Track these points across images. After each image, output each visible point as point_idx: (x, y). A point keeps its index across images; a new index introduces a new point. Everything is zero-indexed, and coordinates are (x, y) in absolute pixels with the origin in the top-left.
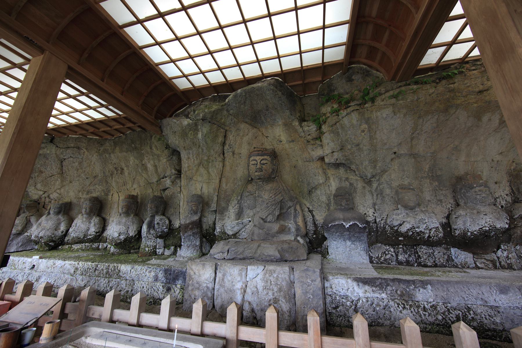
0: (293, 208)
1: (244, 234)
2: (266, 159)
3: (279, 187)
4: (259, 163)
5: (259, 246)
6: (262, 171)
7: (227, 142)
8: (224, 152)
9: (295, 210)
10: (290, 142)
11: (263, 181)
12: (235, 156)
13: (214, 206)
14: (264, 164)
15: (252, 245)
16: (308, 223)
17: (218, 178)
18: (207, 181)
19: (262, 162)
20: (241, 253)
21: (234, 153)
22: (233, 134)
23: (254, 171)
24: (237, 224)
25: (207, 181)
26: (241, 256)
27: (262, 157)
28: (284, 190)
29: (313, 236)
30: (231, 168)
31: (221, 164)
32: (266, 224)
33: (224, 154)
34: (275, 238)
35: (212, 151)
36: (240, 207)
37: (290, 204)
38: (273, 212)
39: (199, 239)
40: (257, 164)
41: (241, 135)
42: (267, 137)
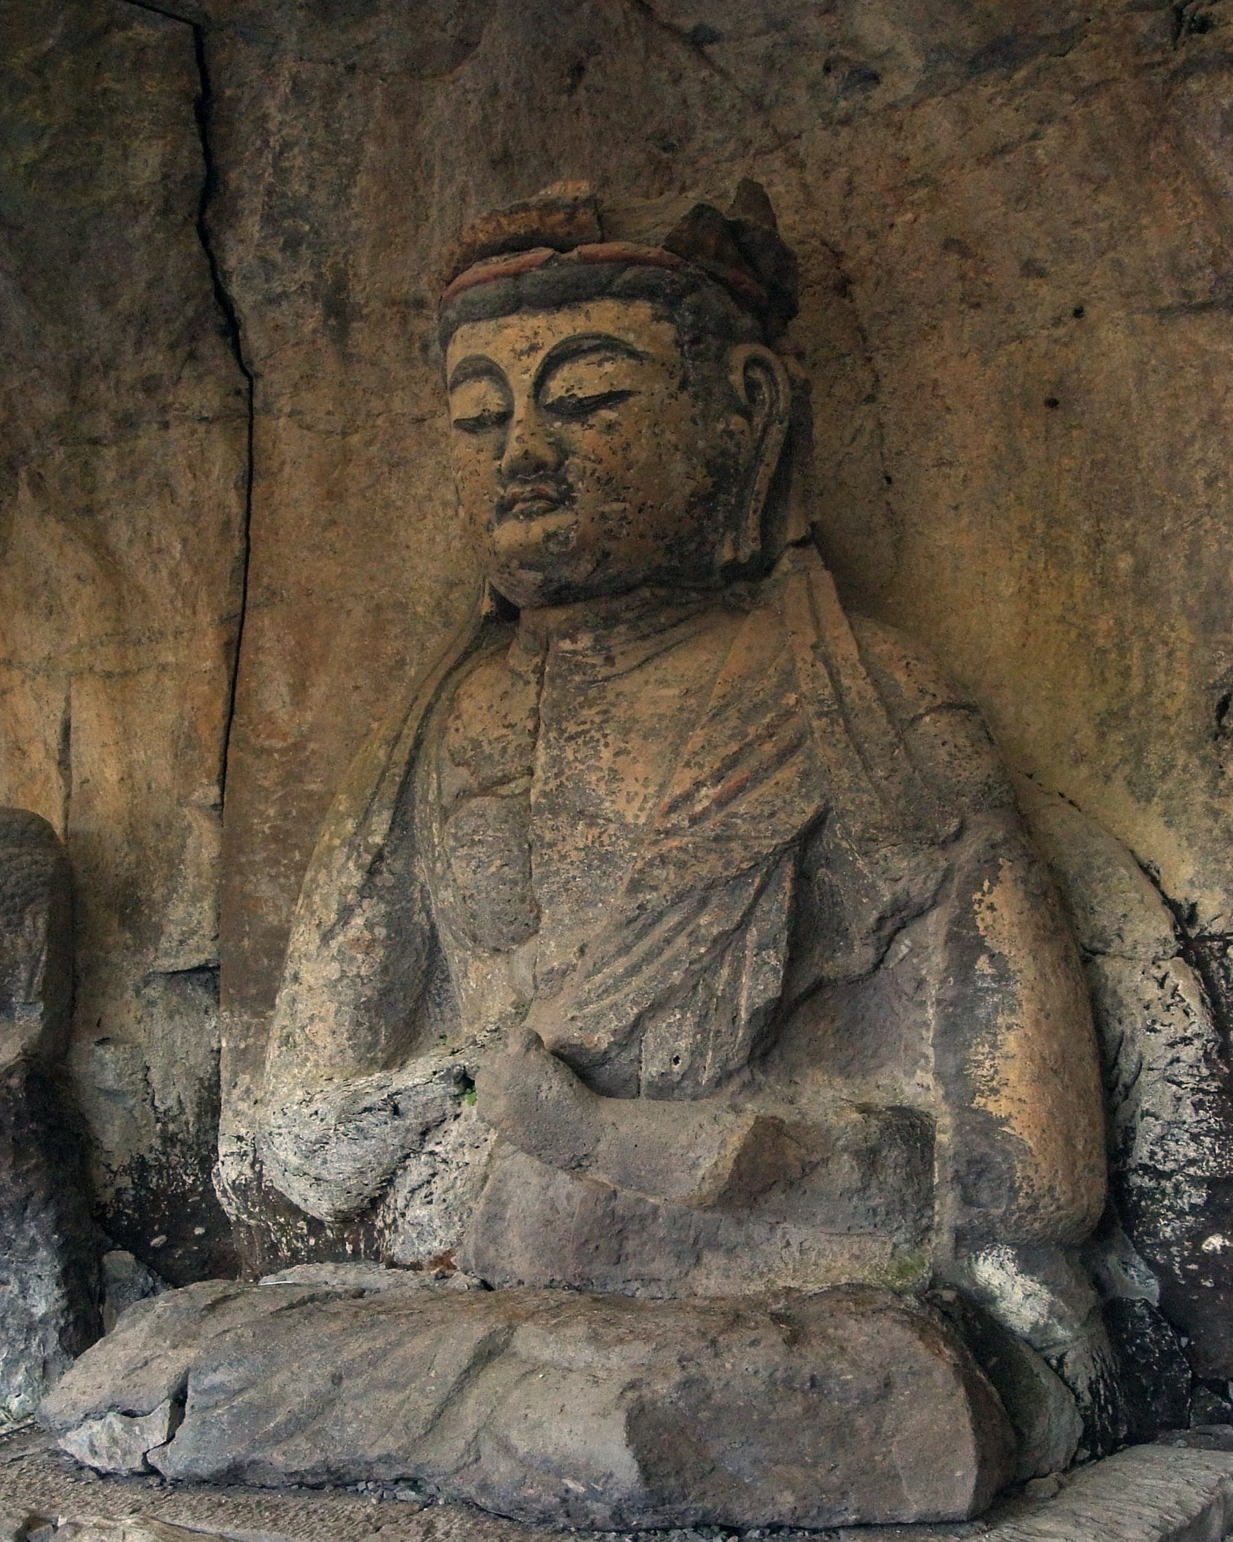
0: (936, 924)
1: (421, 1223)
2: (608, 346)
3: (788, 680)
4: (521, 407)
5: (487, 1354)
6: (564, 500)
7: (248, 181)
8: (225, 304)
9: (965, 944)
10: (976, 65)
11: (610, 621)
12: (361, 338)
13: (187, 926)
14: (580, 409)
15: (418, 1345)
16: (1154, 1096)
17: (205, 618)
18: (107, 658)
19: (556, 387)
20: (297, 1425)
21: (339, 310)
22: (288, 67)
24: (345, 1117)
25: (107, 658)
26: (301, 1456)
28: (839, 708)
29: (1198, 1237)
30: (335, 494)
31: (222, 458)
32: (608, 1110)
33: (232, 329)
34: (713, 1260)
35: (89, 308)
36: (398, 924)
37: (899, 872)
38: (702, 972)
39: (46, 1264)
40: (503, 418)
41: (390, 60)
42: (699, 40)
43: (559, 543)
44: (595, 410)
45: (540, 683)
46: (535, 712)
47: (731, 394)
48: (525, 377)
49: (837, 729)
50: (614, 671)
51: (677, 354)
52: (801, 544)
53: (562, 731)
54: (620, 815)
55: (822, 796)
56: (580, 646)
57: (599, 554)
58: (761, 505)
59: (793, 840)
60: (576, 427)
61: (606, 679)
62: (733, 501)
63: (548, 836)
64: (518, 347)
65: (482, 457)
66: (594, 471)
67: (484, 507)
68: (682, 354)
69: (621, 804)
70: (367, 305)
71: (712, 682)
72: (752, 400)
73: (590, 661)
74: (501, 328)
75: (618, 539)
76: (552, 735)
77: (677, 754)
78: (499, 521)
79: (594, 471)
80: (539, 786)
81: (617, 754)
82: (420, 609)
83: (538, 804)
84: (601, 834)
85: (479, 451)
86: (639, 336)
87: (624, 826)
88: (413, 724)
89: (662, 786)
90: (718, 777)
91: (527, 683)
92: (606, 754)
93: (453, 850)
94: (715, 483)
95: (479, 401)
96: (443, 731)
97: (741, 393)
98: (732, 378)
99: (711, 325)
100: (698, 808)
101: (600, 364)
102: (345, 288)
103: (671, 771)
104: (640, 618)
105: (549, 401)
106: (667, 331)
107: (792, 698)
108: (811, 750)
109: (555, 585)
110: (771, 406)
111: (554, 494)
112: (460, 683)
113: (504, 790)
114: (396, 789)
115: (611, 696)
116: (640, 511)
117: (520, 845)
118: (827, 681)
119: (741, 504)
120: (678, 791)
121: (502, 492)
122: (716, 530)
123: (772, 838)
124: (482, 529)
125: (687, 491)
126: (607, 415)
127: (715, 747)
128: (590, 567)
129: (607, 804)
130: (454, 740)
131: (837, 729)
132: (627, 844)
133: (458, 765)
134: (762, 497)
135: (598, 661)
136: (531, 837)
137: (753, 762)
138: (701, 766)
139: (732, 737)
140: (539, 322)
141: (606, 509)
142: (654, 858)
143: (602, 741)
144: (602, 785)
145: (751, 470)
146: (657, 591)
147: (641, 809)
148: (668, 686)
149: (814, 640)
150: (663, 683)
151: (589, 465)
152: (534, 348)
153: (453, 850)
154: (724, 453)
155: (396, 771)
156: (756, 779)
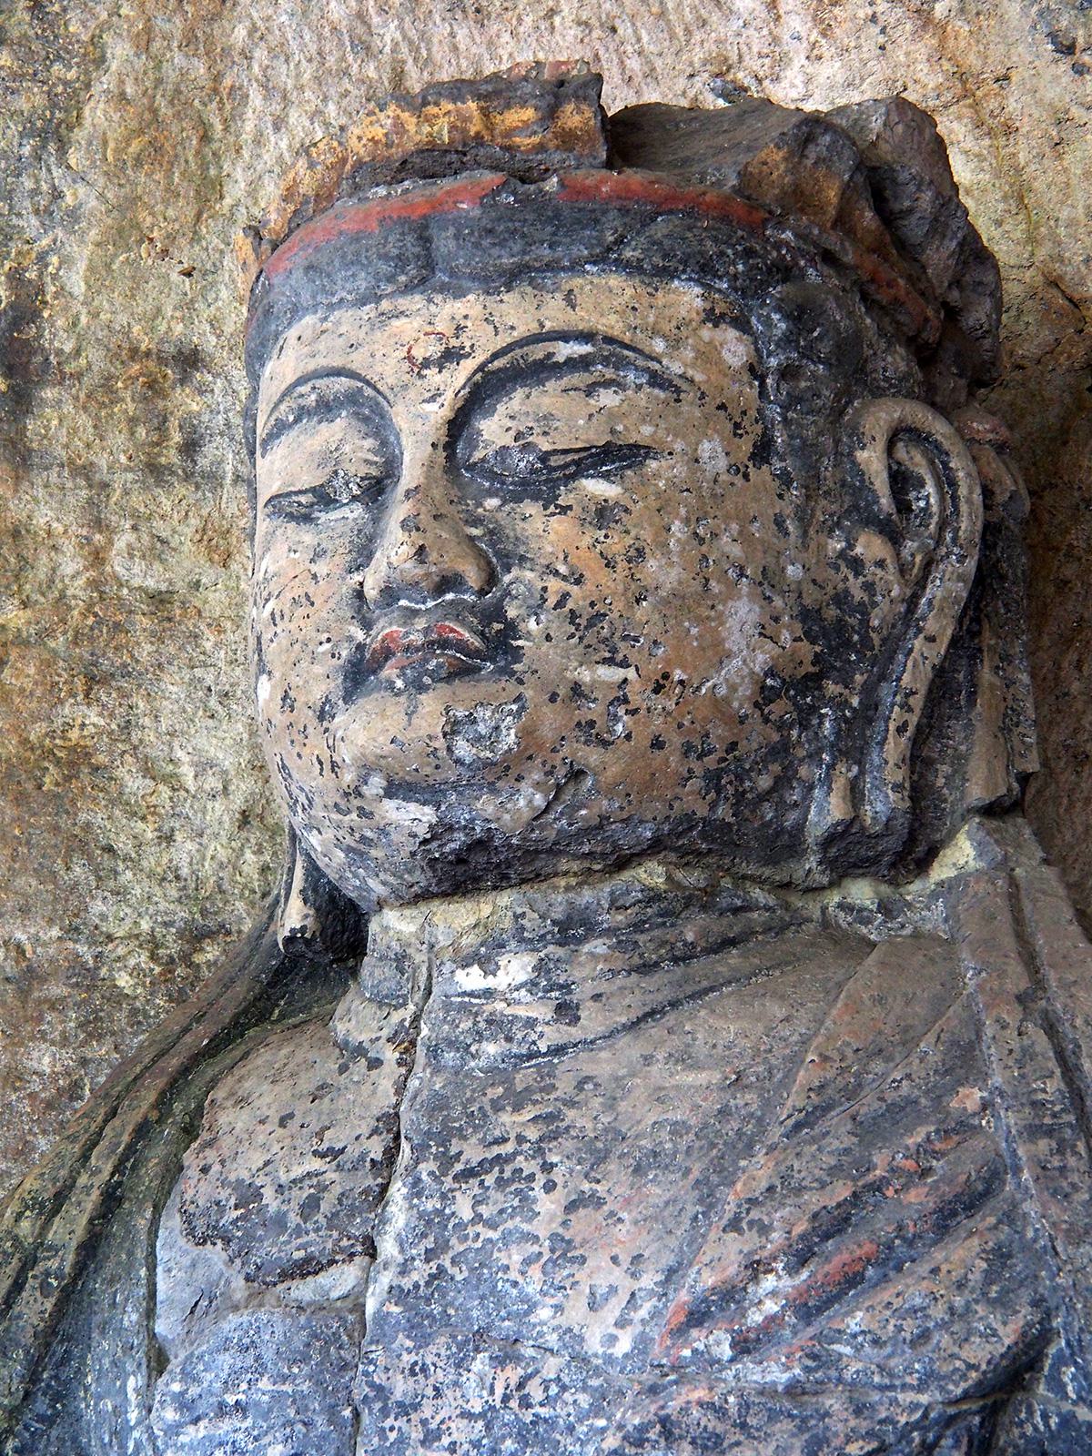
11: (572, 930)
14: (547, 479)
23: (320, 682)
27: (518, 313)
40: (376, 490)
43: (478, 740)
44: (573, 477)
45: (406, 1063)
46: (390, 1122)
47: (858, 488)
48: (433, 407)
49: (1072, 1161)
50: (575, 1033)
51: (752, 392)
52: (991, 811)
53: (447, 1161)
54: (572, 1337)
55: (1035, 1304)
56: (500, 981)
57: (561, 772)
58: (914, 719)
59: (966, 1396)
60: (531, 508)
61: (559, 1050)
62: (855, 702)
63: (401, 1387)
64: (419, 353)
65: (321, 568)
66: (565, 596)
67: (318, 669)
68: (763, 393)
69: (576, 1313)
70: (77, 352)
71: (795, 1060)
72: (903, 507)
73: (522, 1012)
74: (385, 317)
75: (605, 744)
76: (425, 1169)
77: (709, 1202)
78: (348, 697)
79: (565, 596)
80: (386, 1279)
81: (571, 1207)
82: (124, 981)
83: (381, 1318)
84: (528, 1377)
85: (318, 554)
86: (675, 343)
87: (580, 1359)
88: (103, 1164)
89: (672, 1274)
90: (801, 1256)
91: (375, 1064)
92: (548, 1205)
93: (174, 1430)
94: (817, 659)
95: (330, 458)
96: (174, 1170)
97: (881, 484)
98: (862, 456)
99: (825, 348)
100: (755, 1318)
101: (590, 391)
102: (35, 315)
103: (695, 1241)
104: (638, 927)
105: (478, 455)
106: (734, 349)
107: (971, 1097)
108: (1015, 1205)
109: (458, 841)
110: (942, 527)
111: (475, 642)
112: (213, 1083)
113: (304, 1290)
114: (49, 1305)
115: (564, 1086)
116: (658, 689)
117: (332, 1412)
118: (1052, 1064)
119: (871, 708)
120: (709, 1280)
121: (360, 635)
122: (814, 757)
123: (920, 1389)
124: (309, 717)
125: (761, 660)
126: (597, 488)
127: (800, 1190)
128: (539, 801)
129: (544, 1313)
130: (195, 1189)
131: (1072, 1161)
132: (584, 1400)
133: (202, 1242)
134: (917, 702)
135: (543, 1012)
136: (360, 1390)
137: (884, 1226)
138: (764, 1230)
139: (834, 1171)
140: (470, 306)
141: (585, 676)
142: (643, 1429)
143: (541, 1179)
144: (535, 1272)
145: (894, 644)
146: (679, 875)
147: (622, 1323)
148: (697, 1066)
149: (1024, 984)
150: (684, 1059)
151: (554, 585)
152: (451, 355)
153: (174, 1430)
154: (841, 599)
155: (53, 1264)
156: (889, 1261)
